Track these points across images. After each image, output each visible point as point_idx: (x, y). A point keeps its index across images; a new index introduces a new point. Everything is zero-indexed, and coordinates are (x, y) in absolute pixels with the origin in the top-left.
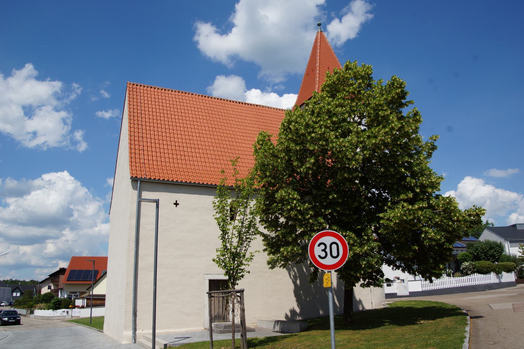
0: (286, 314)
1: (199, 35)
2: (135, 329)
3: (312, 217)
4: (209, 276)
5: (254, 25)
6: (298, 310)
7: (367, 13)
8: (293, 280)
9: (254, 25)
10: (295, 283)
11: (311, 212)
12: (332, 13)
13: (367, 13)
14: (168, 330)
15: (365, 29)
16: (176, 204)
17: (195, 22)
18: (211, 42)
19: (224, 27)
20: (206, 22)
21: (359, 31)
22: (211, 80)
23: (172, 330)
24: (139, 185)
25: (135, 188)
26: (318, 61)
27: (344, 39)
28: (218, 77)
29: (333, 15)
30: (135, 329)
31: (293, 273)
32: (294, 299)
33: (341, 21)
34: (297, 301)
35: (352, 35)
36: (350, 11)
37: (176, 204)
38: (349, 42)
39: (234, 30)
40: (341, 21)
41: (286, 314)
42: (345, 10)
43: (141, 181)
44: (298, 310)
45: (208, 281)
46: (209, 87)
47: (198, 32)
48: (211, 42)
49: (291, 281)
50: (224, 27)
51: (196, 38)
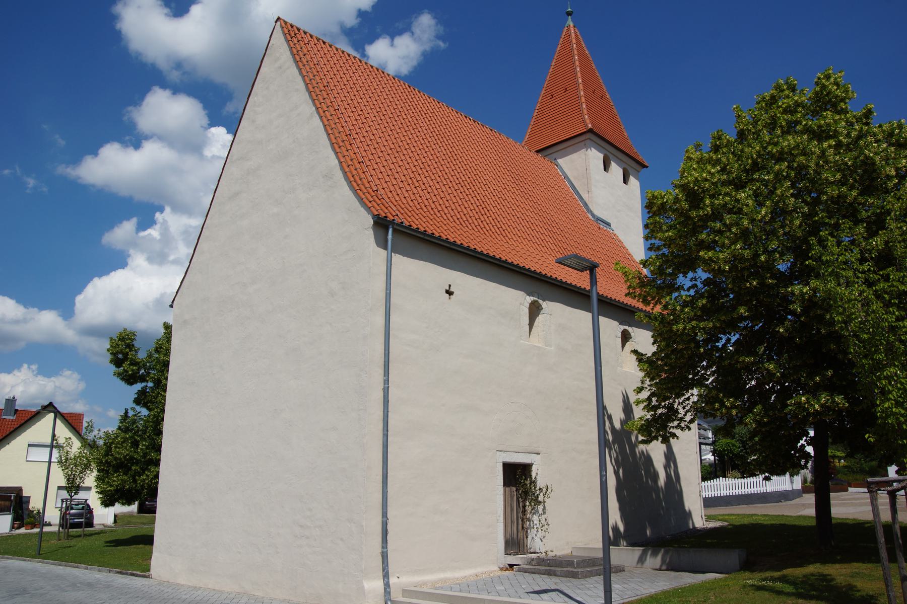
2: (386, 576)
7: (438, 37)
13: (438, 37)
16: (449, 293)
22: (137, 96)
23: (448, 575)
30: (386, 576)
35: (405, 70)
36: (407, 29)
37: (449, 293)
40: (392, 45)
43: (394, 230)
46: (130, 108)
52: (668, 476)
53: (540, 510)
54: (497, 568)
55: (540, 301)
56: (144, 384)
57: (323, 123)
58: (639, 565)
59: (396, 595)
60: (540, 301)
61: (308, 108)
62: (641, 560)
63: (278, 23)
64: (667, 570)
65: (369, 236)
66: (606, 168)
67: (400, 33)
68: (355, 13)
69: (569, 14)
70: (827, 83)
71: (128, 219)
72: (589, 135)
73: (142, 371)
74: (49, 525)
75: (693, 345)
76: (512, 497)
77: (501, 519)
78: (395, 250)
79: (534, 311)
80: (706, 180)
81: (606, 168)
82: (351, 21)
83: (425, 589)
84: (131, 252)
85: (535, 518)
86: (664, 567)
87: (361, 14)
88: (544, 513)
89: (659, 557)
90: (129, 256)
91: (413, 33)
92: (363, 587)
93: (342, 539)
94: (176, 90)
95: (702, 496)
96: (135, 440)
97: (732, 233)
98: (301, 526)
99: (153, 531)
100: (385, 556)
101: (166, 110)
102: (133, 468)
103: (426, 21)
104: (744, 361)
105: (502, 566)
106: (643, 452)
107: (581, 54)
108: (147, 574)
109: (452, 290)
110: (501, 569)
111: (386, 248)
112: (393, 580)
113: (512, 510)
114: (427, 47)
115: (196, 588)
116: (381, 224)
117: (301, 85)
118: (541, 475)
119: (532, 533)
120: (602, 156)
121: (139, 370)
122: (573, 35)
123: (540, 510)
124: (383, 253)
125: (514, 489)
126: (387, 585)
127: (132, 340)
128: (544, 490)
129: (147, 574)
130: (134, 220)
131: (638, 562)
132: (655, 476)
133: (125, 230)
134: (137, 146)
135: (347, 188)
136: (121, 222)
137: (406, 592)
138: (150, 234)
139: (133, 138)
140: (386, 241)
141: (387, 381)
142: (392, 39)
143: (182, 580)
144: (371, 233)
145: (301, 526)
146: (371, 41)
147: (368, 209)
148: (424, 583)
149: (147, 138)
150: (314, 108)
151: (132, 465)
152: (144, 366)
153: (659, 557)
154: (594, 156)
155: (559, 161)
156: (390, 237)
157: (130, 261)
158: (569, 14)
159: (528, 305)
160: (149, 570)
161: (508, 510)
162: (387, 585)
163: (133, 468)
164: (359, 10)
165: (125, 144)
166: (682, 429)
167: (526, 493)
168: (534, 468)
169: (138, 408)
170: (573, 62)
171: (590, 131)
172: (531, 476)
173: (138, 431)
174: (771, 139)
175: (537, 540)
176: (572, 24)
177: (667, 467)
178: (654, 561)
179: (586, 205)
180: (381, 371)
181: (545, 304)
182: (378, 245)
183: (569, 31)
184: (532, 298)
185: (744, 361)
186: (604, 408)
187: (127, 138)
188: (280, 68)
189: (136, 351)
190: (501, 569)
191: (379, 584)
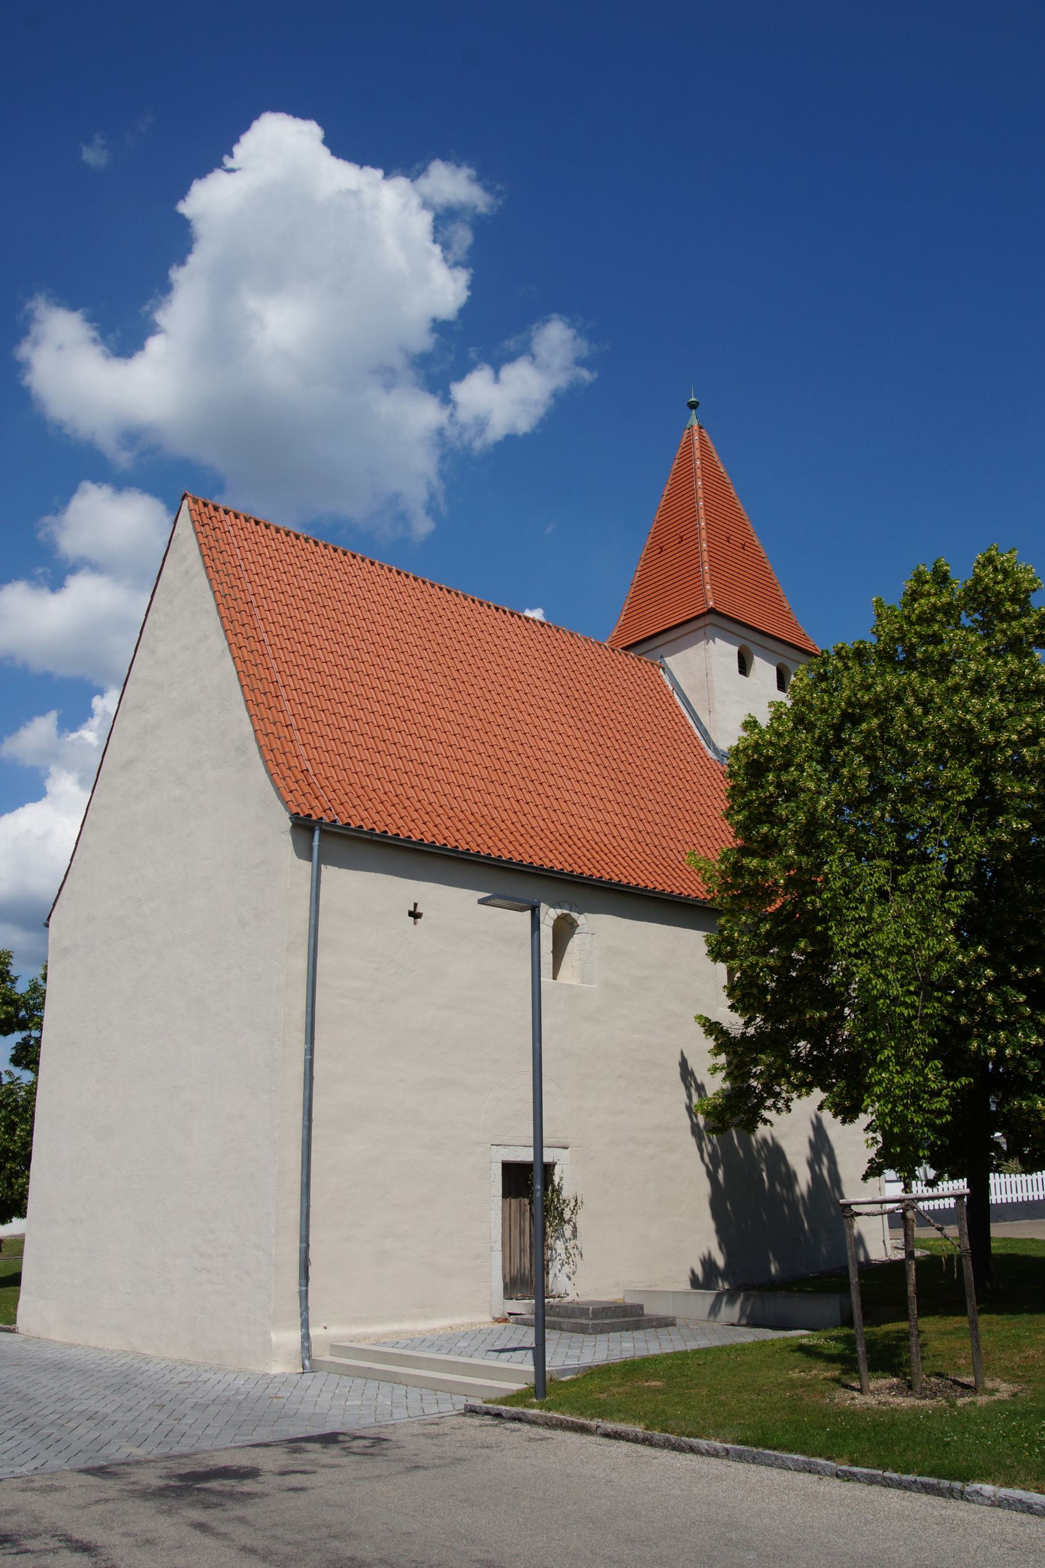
0: (693, 1272)
1: (36, 343)
2: (305, 1324)
3: (992, 985)
4: (505, 1150)
5: (221, 344)
6: (720, 1261)
7: (579, 362)
8: (707, 1167)
9: (221, 344)
10: (712, 1176)
11: (989, 972)
12: (471, 349)
13: (579, 362)
14: (396, 1327)
15: (565, 408)
16: (415, 915)
17: (30, 295)
18: (72, 370)
19: (123, 332)
20: (73, 307)
21: (547, 413)
22: (58, 495)
23: (407, 1326)
24: (316, 843)
25: (304, 852)
26: (702, 512)
27: (497, 430)
28: (87, 485)
29: (473, 355)
30: (305, 1324)
31: (710, 1148)
32: (710, 1225)
33: (497, 379)
34: (719, 1231)
35: (524, 425)
36: (525, 350)
37: (415, 915)
38: (511, 441)
39: (155, 345)
40: (497, 379)
41: (693, 1272)
42: (510, 344)
43: (323, 832)
44: (720, 1261)
45: (500, 1165)
46: (47, 519)
47: (35, 329)
48: (72, 370)
49: (703, 1169)
50: (123, 332)
51: (24, 350)
52: (816, 1178)
53: (568, 1233)
54: (489, 1319)
55: (575, 915)
56: (25, 1034)
57: (236, 668)
58: (712, 1318)
59: (321, 1353)
60: (575, 915)
61: (218, 642)
62: (714, 1310)
63: (185, 502)
64: (747, 1325)
65: (285, 842)
66: (744, 668)
67: (511, 358)
68: (426, 325)
69: (693, 406)
70: (982, 574)
71: (43, 713)
72: (709, 619)
73: (23, 1013)
74: (553, 1297)
75: (755, 991)
76: (522, 1214)
77: (498, 1246)
78: (325, 859)
79: (564, 931)
80: (771, 743)
81: (744, 668)
82: (422, 341)
83: (363, 1345)
84: (53, 769)
85: (559, 1245)
86: (744, 1321)
87: (439, 326)
88: (575, 1236)
89: (738, 1306)
90: (48, 776)
91: (533, 357)
92: (270, 1339)
93: (248, 1273)
94: (121, 482)
95: (884, 1210)
96: (12, 1121)
97: (790, 830)
98: (202, 1255)
99: (21, 1266)
100: (304, 1296)
101: (108, 520)
102: (8, 1166)
103: (555, 337)
104: (812, 1018)
105: (498, 1316)
106: (765, 1140)
107: (711, 476)
108: (12, 1327)
109: (419, 910)
110: (497, 1320)
111: (310, 859)
112: (314, 1332)
113: (522, 1233)
114: (561, 381)
115: (72, 1346)
116: (303, 826)
117: (211, 605)
118: (568, 1177)
119: (554, 1268)
120: (735, 650)
121: (18, 1010)
122: (697, 444)
123: (568, 1233)
124: (306, 867)
125: (526, 1201)
126: (306, 1337)
127: (7, 964)
128: (572, 1203)
129: (12, 1327)
130: (53, 716)
131: (710, 1314)
132: (791, 1178)
133: (41, 730)
134: (56, 583)
135: (262, 769)
136: (30, 719)
137: (337, 1349)
138: (81, 737)
139: (52, 572)
140: (311, 848)
141: (310, 1050)
142: (497, 372)
143: (55, 1336)
144: (288, 838)
145: (202, 1255)
146: (460, 377)
147: (286, 803)
148: (366, 1337)
149: (74, 569)
150: (226, 643)
151: (7, 1161)
152: (26, 1005)
153: (738, 1306)
154: (722, 652)
155: (668, 660)
156: (316, 843)
157: (49, 785)
158: (693, 406)
159: (552, 923)
160: (15, 1323)
161: (515, 1232)
162: (306, 1337)
163: (8, 1166)
164: (434, 320)
165: (35, 581)
166: (779, 1110)
167: (546, 1209)
168: (557, 1170)
169: (17, 1071)
170: (693, 490)
171: (712, 611)
172: (552, 1181)
173: (17, 1107)
174: (863, 680)
175: (562, 1277)
176: (695, 424)
177: (813, 1163)
178: (731, 1312)
179: (705, 733)
180: (302, 1036)
181: (581, 919)
182: (299, 855)
183: (690, 436)
184: (559, 911)
185: (812, 1018)
186: (692, 1074)
187: (40, 570)
188: (187, 572)
189: (13, 982)
190: (497, 1320)
191: (295, 1336)
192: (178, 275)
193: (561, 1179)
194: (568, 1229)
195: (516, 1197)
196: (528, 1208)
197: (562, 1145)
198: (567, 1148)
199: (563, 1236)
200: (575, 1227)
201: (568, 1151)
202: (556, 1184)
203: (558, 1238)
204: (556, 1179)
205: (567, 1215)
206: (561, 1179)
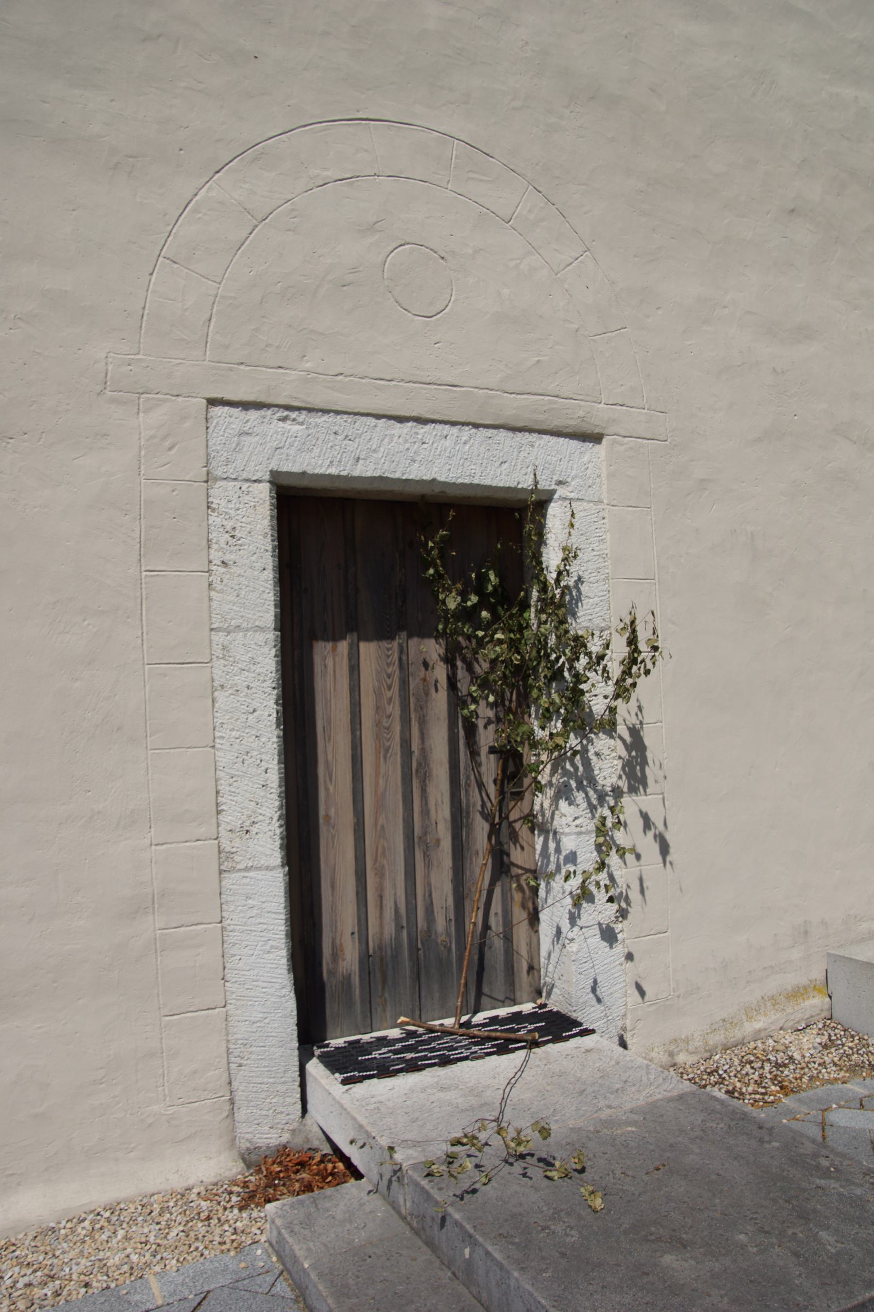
4: (270, 428)
45: (263, 493)
76: (411, 707)
113: (414, 772)
128: (619, 650)
168: (555, 518)
170: (370, 1071)
192: (494, 485)
193: (569, 555)
194: (607, 758)
195: (384, 634)
196: (440, 672)
197: (571, 423)
198: (596, 438)
199: (588, 779)
200: (636, 743)
201: (601, 450)
202: (552, 577)
203: (563, 793)
204: (552, 558)
205: (598, 697)
206: (569, 555)
